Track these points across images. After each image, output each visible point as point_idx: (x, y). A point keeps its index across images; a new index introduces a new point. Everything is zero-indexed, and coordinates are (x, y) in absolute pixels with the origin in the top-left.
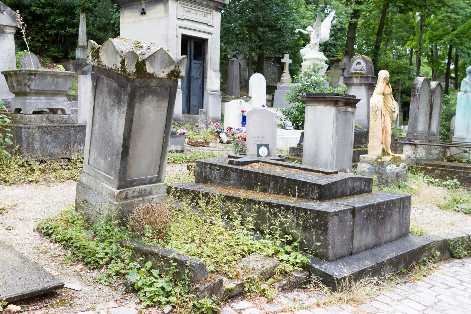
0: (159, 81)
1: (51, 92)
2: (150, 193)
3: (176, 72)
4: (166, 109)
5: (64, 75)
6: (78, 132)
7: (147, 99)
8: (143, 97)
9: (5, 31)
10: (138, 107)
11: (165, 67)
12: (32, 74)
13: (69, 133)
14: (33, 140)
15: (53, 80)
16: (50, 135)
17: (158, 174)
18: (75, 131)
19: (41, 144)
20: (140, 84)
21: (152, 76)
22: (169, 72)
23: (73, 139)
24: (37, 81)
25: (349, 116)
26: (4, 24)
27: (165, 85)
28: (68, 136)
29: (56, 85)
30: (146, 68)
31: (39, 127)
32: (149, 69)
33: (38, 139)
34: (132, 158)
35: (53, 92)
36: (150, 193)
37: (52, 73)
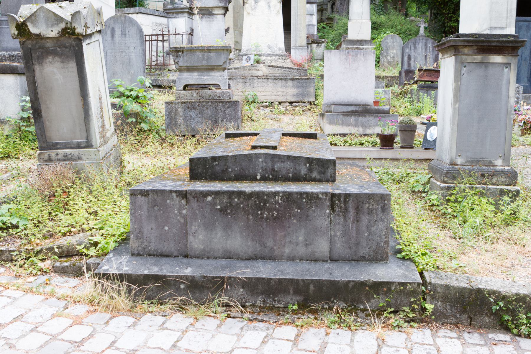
0: (55, 41)
1: (203, 67)
2: (79, 158)
3: (69, 29)
4: (75, 70)
5: (216, 50)
6: (228, 108)
7: (48, 60)
8: (41, 59)
9: (213, 12)
10: (38, 69)
11: (53, 26)
12: (179, 51)
13: (216, 109)
14: (176, 115)
15: (203, 55)
16: (194, 111)
17: (87, 139)
18: (224, 107)
19: (185, 119)
20: (32, 45)
21: (39, 36)
22: (60, 30)
23: (221, 115)
24: (185, 58)
25: (491, 70)
26: (210, 6)
27: (65, 44)
28: (216, 112)
29: (207, 60)
30: (28, 29)
31: (182, 103)
32: (33, 29)
33: (181, 114)
34: (48, 120)
35: (205, 67)
36: (80, 158)
37: (200, 48)
